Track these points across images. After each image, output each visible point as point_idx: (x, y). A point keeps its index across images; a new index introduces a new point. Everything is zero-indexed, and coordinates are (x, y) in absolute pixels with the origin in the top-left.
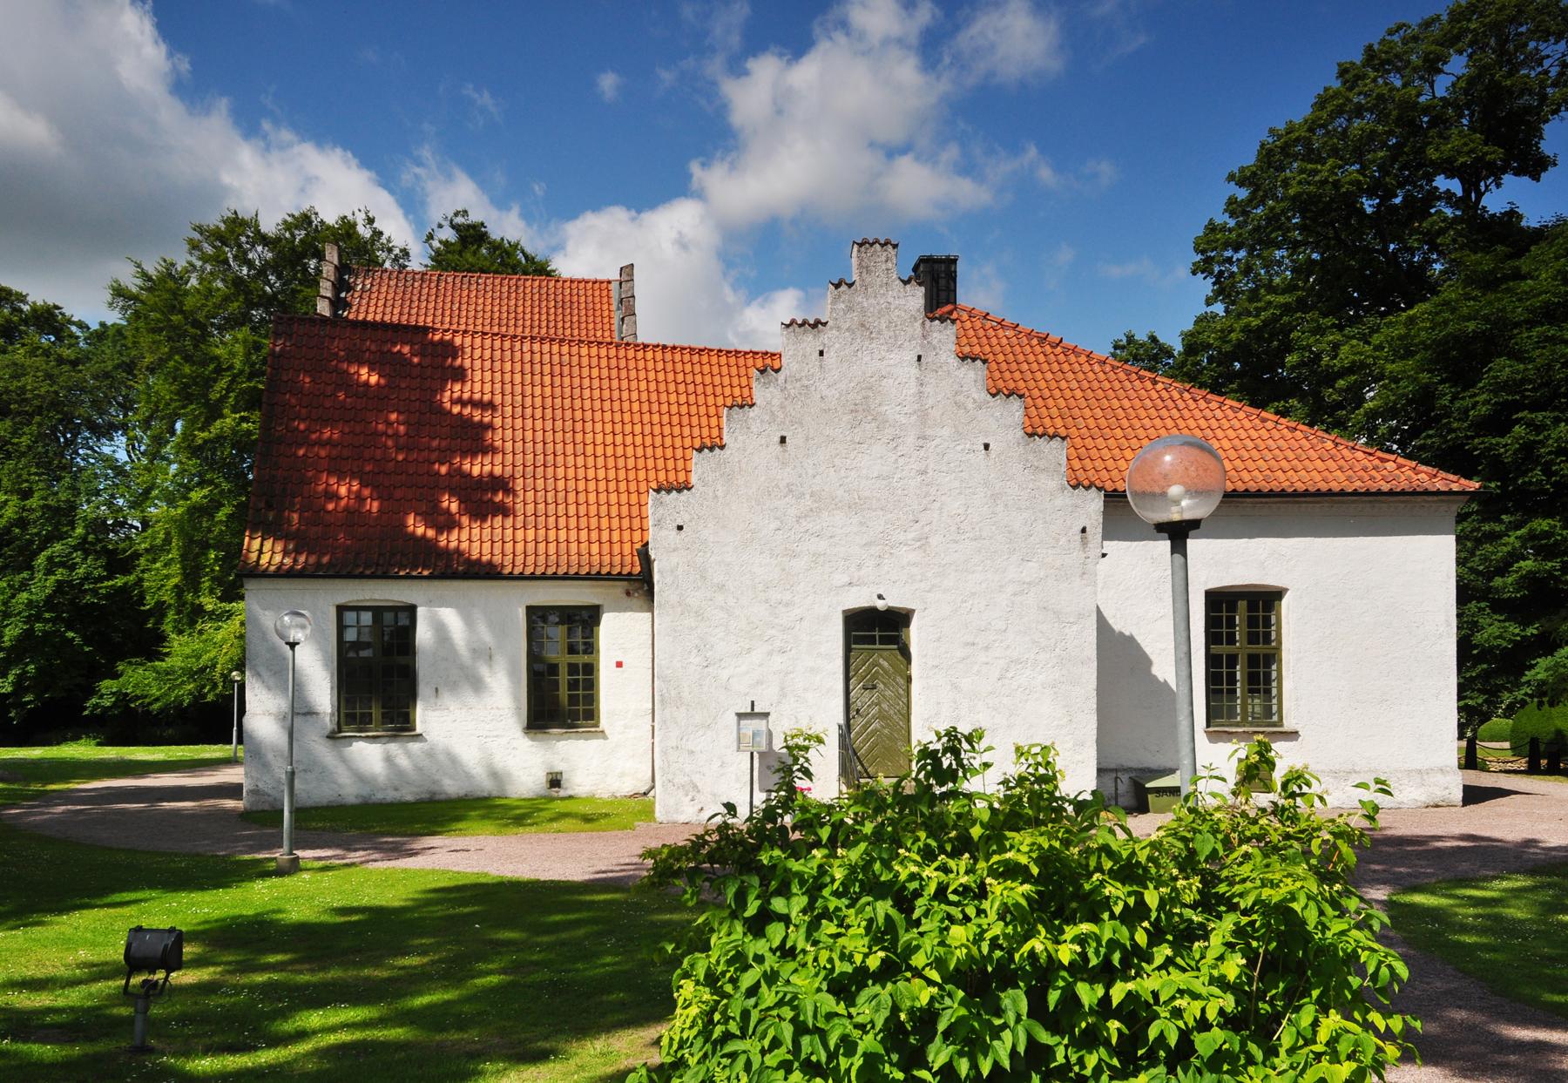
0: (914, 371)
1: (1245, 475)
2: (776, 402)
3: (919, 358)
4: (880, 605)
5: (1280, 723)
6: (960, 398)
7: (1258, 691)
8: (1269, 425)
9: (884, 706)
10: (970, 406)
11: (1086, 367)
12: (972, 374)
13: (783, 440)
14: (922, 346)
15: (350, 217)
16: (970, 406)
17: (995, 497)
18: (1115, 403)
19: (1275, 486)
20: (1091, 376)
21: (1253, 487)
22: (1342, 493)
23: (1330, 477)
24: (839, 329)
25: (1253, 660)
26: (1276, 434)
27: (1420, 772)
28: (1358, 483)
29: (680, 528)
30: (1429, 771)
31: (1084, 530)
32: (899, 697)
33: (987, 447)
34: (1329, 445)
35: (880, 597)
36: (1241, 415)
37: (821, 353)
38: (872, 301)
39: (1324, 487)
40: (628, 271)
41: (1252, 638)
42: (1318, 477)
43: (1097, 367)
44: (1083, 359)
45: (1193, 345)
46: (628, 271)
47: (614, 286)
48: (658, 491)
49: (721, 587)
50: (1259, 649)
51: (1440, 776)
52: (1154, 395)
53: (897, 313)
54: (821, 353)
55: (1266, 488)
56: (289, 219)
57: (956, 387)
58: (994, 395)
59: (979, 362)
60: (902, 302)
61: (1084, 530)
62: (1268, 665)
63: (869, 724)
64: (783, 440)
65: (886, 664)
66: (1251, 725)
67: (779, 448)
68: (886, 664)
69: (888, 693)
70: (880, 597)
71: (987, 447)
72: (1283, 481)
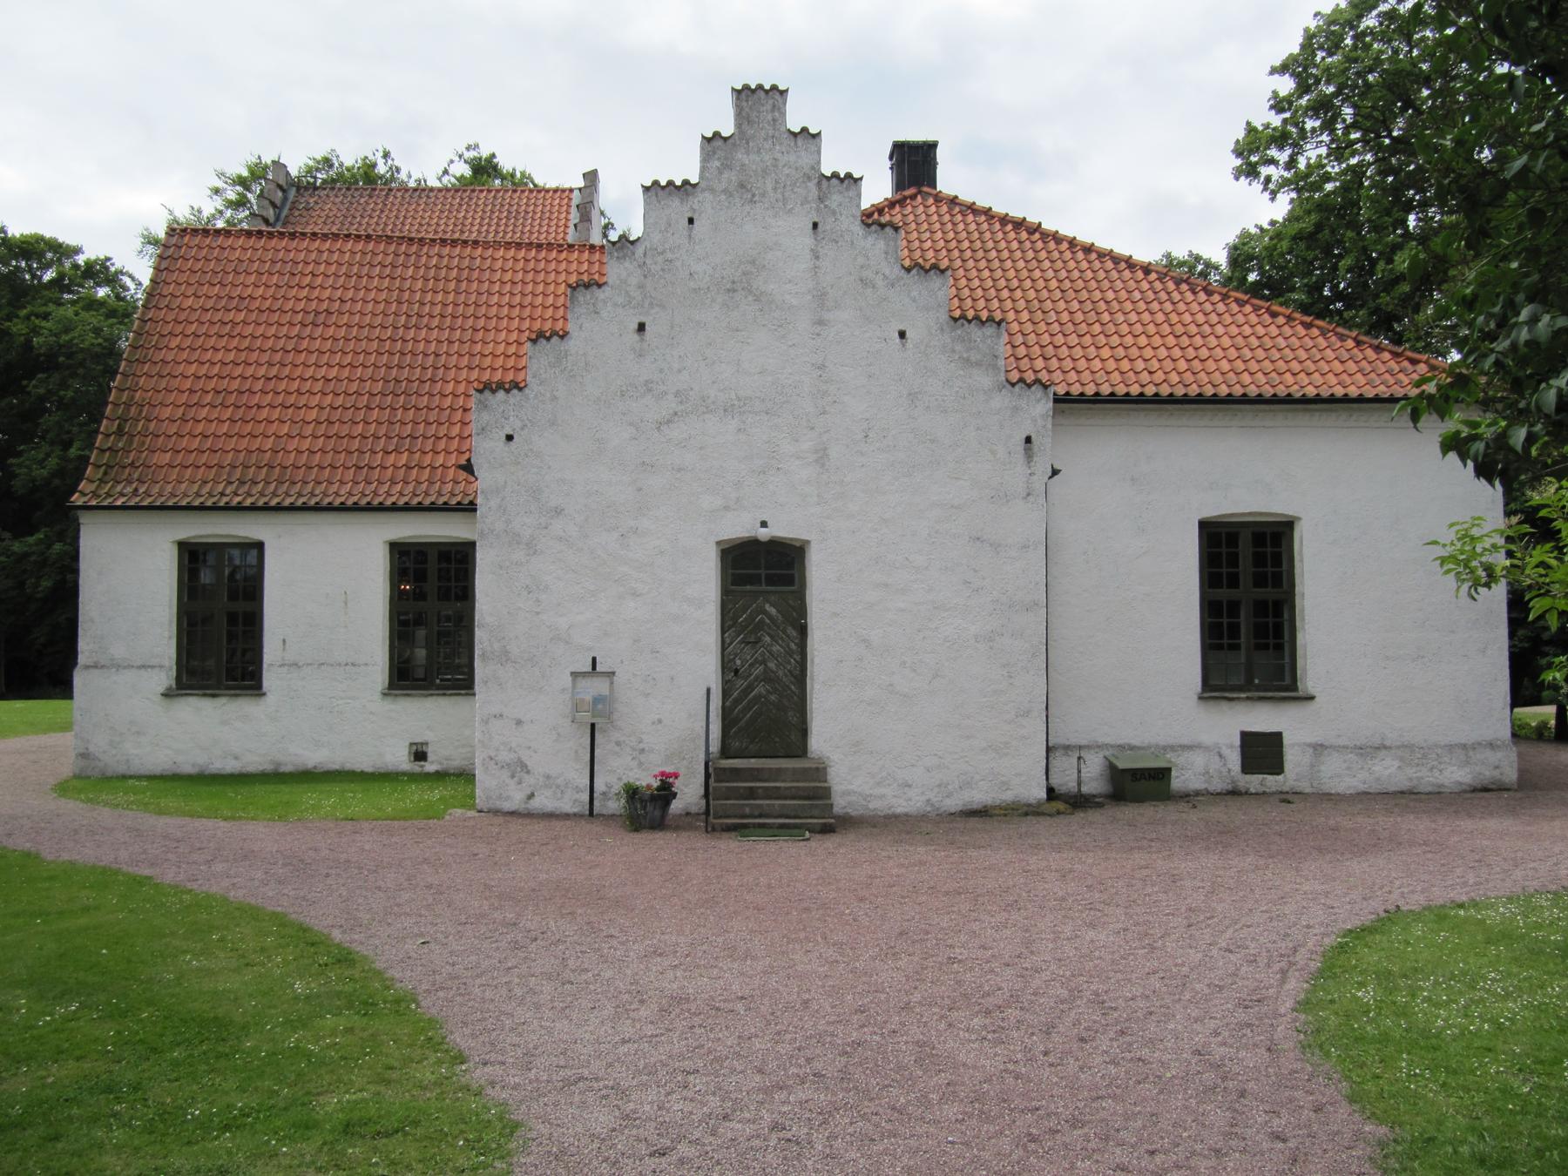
0: (807, 240)
1: (1246, 378)
2: (634, 281)
3: (815, 225)
4: (764, 534)
5: (1296, 689)
6: (865, 274)
7: (1266, 647)
8: (1281, 320)
9: (772, 665)
10: (880, 282)
11: (1068, 255)
12: (881, 244)
13: (641, 327)
14: (818, 210)
15: (371, 157)
16: (880, 282)
17: (913, 396)
18: (1097, 295)
19: (1281, 391)
20: (1072, 264)
21: (1253, 391)
22: (1361, 400)
23: (1348, 380)
24: (712, 190)
25: (1261, 607)
26: (1287, 331)
27: (1464, 747)
28: (1382, 388)
29: (510, 438)
30: (1476, 746)
31: (1028, 440)
32: (790, 653)
33: (902, 335)
34: (1350, 343)
35: (764, 524)
36: (1248, 309)
37: (691, 221)
38: (753, 157)
39: (1339, 391)
40: (591, 177)
41: (1260, 581)
42: (1332, 380)
43: (1080, 255)
44: (1065, 245)
45: (1240, 256)
46: (591, 177)
47: (576, 195)
48: (480, 391)
49: (558, 511)
50: (1268, 593)
51: (1488, 754)
52: (1145, 285)
53: (786, 171)
54: (691, 221)
55: (1268, 392)
56: (311, 163)
57: (861, 260)
58: (908, 270)
59: (888, 230)
60: (792, 158)
61: (1028, 440)
62: (1278, 613)
63: (750, 688)
64: (641, 327)
65: (773, 611)
66: (1258, 688)
67: (636, 337)
68: (773, 611)
69: (776, 648)
70: (764, 524)
71: (902, 335)
72: (1290, 385)
